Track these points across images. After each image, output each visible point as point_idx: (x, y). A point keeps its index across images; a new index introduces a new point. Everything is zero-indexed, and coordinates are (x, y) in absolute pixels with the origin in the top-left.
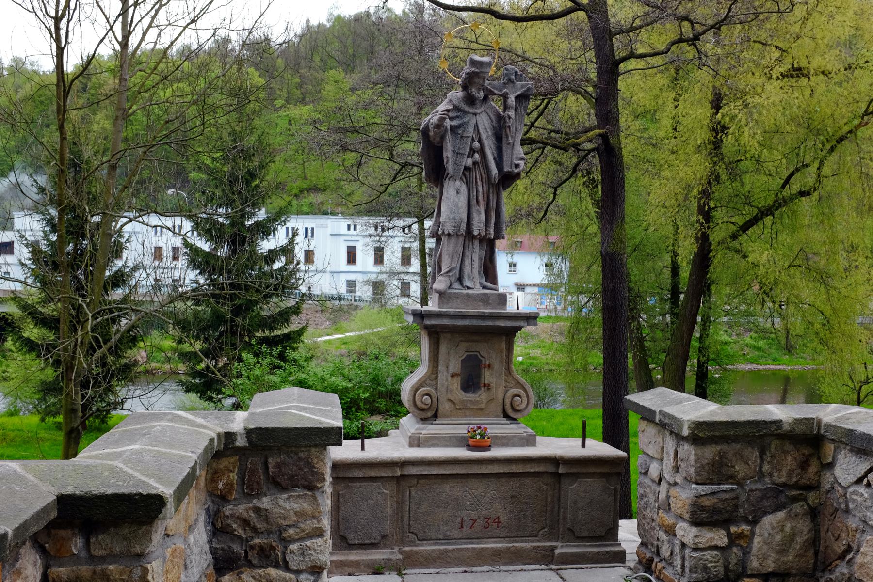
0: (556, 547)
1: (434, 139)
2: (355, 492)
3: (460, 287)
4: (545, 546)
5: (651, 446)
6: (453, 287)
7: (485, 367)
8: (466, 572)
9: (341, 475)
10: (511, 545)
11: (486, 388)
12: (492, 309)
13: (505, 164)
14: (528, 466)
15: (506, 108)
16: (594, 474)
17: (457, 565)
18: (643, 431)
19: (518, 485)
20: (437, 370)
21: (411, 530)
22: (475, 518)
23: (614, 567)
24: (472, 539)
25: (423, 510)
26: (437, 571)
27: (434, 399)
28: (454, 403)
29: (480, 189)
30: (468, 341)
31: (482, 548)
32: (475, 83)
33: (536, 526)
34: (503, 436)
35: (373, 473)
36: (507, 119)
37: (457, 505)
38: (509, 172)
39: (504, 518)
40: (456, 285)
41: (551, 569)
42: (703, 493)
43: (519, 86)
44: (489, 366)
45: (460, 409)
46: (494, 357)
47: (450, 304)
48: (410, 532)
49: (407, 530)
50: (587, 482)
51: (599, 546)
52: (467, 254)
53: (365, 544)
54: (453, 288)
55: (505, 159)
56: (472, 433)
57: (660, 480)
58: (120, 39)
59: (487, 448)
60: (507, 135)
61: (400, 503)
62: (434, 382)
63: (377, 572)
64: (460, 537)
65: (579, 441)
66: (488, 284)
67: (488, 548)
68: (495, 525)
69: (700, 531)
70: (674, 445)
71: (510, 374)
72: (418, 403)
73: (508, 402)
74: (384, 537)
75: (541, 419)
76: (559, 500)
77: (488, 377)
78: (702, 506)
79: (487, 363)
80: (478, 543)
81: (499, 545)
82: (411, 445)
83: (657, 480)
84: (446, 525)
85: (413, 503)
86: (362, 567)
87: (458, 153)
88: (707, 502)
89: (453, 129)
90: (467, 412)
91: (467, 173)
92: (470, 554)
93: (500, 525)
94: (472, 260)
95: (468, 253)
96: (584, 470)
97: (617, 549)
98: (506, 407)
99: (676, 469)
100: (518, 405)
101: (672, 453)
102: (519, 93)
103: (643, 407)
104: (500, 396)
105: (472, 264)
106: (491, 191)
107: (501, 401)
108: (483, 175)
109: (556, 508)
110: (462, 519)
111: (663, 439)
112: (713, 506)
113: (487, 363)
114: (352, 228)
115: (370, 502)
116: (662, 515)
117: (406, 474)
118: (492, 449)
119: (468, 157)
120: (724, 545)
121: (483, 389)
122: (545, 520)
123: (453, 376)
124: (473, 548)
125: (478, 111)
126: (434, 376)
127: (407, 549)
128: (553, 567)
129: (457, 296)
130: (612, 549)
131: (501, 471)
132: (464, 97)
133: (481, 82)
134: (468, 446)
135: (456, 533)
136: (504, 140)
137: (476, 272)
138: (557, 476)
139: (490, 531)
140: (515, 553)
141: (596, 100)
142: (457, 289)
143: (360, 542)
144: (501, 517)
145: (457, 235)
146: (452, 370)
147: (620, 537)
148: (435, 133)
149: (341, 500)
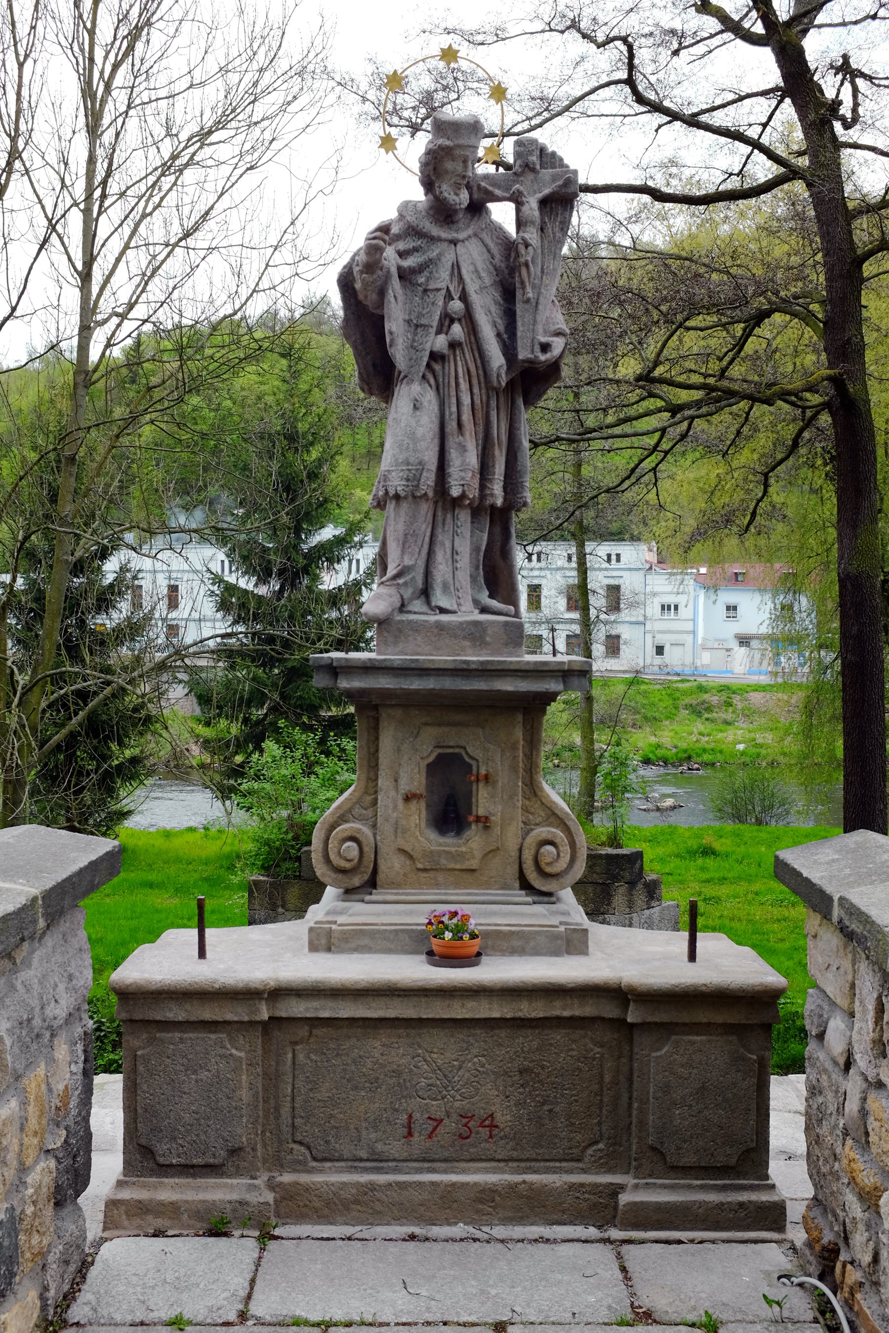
0: (622, 1187)
1: (366, 297)
3: (425, 609)
4: (597, 1185)
5: (830, 975)
6: (410, 608)
7: (478, 780)
8: (413, 1237)
9: (138, 1016)
10: (518, 1178)
11: (480, 825)
12: (491, 655)
13: (519, 343)
14: (558, 1003)
16: (709, 1024)
17: (398, 1220)
18: (815, 937)
19: (535, 1044)
21: (299, 1138)
22: (439, 1115)
23: (756, 1242)
24: (433, 1161)
26: (348, 1230)
27: (366, 849)
28: (411, 857)
29: (466, 400)
30: (439, 725)
31: (454, 1185)
32: (447, 172)
33: (579, 1137)
34: (512, 933)
35: (208, 1013)
36: (522, 249)
39: (503, 1118)
40: (418, 605)
41: (607, 1241)
43: (547, 178)
44: (487, 777)
45: (425, 870)
46: (498, 758)
47: (401, 645)
48: (295, 1142)
49: (289, 1136)
50: (693, 1043)
52: (440, 537)
53: (193, 1166)
54: (410, 612)
55: (519, 334)
56: (438, 926)
58: (80, 267)
59: (471, 960)
60: (522, 283)
63: (217, 1231)
66: (494, 604)
67: (467, 1184)
68: (484, 1132)
70: (876, 985)
71: (536, 795)
72: (332, 856)
73: (528, 856)
74: (234, 1152)
75: (758, 843)
76: (630, 1080)
79: (483, 771)
80: (445, 1172)
81: (492, 1178)
82: (314, 947)
83: (842, 1061)
84: (376, 1128)
86: (185, 1217)
87: (417, 326)
89: (404, 275)
90: (441, 878)
91: (437, 367)
92: (426, 1196)
93: (495, 1131)
94: (454, 552)
95: (444, 538)
96: (685, 1017)
97: (764, 1197)
98: (524, 866)
100: (549, 864)
101: (871, 1007)
103: (807, 880)
104: (512, 844)
105: (454, 561)
106: (493, 403)
107: (515, 854)
110: (410, 1117)
111: (853, 965)
113: (483, 771)
115: (204, 1075)
116: (852, 1155)
117: (284, 1014)
118: (484, 959)
119: (439, 332)
121: (473, 827)
122: (599, 1124)
123: (407, 799)
125: (461, 236)
126: (369, 798)
127: (287, 1178)
128: (615, 1234)
129: (417, 628)
131: (496, 1014)
132: (431, 208)
133: (460, 168)
134: (430, 953)
135: (395, 1148)
138: (620, 1024)
139: (473, 1145)
140: (528, 1198)
141: (825, 324)
142: (419, 613)
143: (182, 1161)
144: (498, 1116)
145: (414, 497)
146: (405, 785)
147: (771, 1171)
148: (366, 285)
149: (141, 1068)
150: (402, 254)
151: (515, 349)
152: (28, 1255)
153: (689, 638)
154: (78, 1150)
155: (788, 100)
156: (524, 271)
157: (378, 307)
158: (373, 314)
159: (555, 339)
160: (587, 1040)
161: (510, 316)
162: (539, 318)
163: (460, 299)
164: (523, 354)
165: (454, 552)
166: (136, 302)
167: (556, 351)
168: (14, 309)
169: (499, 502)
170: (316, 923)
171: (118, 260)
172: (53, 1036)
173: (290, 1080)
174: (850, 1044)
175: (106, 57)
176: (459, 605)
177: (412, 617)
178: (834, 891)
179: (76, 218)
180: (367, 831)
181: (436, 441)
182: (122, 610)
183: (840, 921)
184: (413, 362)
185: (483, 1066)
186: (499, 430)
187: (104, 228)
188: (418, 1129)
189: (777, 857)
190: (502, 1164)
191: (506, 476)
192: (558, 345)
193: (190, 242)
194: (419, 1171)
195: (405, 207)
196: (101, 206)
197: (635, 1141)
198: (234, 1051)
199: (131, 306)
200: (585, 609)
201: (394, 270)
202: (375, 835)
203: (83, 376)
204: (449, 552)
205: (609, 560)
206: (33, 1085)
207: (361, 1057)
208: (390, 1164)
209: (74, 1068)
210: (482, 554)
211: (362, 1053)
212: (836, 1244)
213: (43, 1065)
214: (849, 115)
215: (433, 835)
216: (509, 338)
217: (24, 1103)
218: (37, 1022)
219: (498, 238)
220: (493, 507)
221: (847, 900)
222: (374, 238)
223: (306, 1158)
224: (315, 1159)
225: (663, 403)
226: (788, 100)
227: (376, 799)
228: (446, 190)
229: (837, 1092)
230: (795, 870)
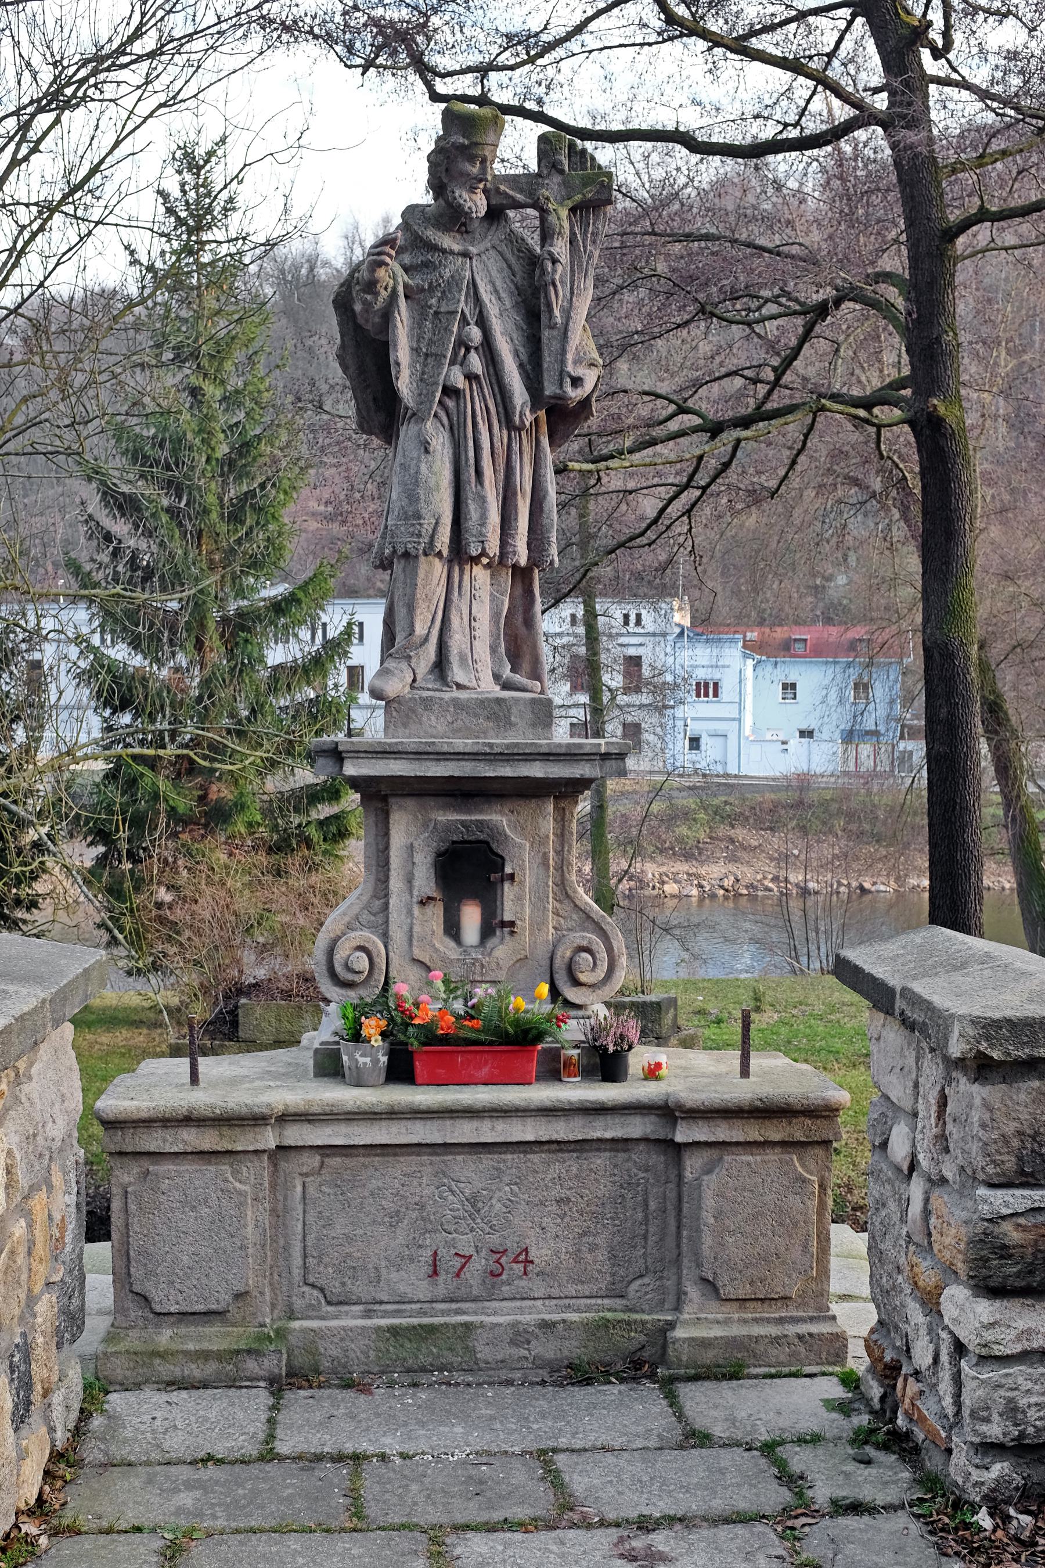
1: (367, 321)
15: (546, 235)
20: (387, 888)
21: (311, 1279)
27: (376, 960)
37: (423, 1219)
42: (1005, 1211)
48: (306, 1284)
55: (545, 366)
57: (912, 1168)
62: (380, 919)
65: (734, 1057)
72: (339, 968)
78: (1004, 1247)
83: (905, 1168)
88: (1011, 1234)
91: (450, 403)
93: (530, 1267)
94: (472, 618)
98: (556, 976)
99: (942, 1141)
107: (546, 963)
110: (436, 1253)
114: (633, 618)
119: (452, 363)
121: (498, 933)
126: (378, 904)
130: (815, 1328)
149: (132, 1207)
154: (73, 1291)
155: (860, 20)
157: (381, 332)
158: (374, 340)
159: (587, 371)
163: (477, 324)
169: (523, 561)
170: (322, 1044)
173: (301, 1217)
174: (914, 1145)
176: (478, 679)
178: (894, 981)
183: (902, 1013)
184: (424, 396)
188: (445, 1266)
189: (838, 956)
191: (531, 530)
195: (411, 212)
198: (237, 1185)
200: (595, 690)
204: (466, 618)
207: (379, 1189)
208: (414, 1306)
210: (503, 621)
211: (380, 1184)
212: (898, 1361)
214: (940, 43)
216: (533, 369)
217: (30, 1226)
219: (519, 251)
220: (515, 567)
221: (909, 990)
223: (320, 1303)
225: (700, 421)
226: (860, 20)
229: (900, 1199)
230: (856, 967)
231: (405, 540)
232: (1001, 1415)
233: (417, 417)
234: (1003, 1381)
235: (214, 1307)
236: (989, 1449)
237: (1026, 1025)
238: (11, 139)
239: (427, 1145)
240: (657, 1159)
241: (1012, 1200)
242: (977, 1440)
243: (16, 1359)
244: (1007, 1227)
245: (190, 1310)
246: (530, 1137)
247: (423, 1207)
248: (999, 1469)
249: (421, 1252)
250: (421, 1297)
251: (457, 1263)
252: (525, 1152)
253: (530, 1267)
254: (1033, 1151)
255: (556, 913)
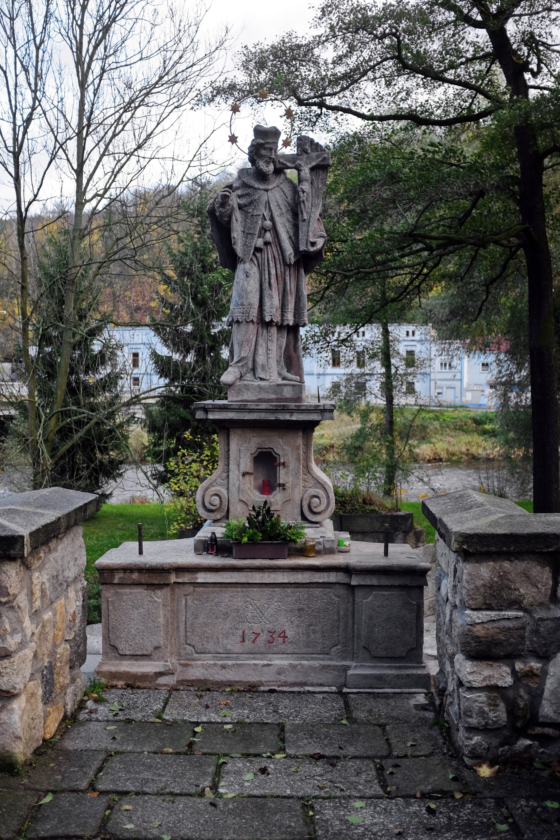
0: (348, 667)
2: (124, 599)
3: (253, 378)
4: (337, 666)
5: (443, 558)
11: (281, 488)
21: (189, 642)
25: (201, 620)
27: (223, 500)
29: (273, 272)
33: (328, 643)
37: (238, 616)
38: (305, 251)
40: (249, 376)
51: (400, 668)
58: (75, 167)
61: (175, 613)
64: (241, 651)
66: (289, 376)
68: (281, 640)
69: (476, 666)
72: (207, 504)
77: (283, 476)
80: (261, 659)
83: (445, 599)
85: (189, 612)
88: (479, 631)
89: (240, 207)
91: (258, 255)
93: (286, 640)
102: (314, 164)
105: (268, 354)
106: (287, 273)
108: (277, 256)
109: (350, 622)
110: (244, 632)
112: (492, 637)
119: (259, 237)
120: (506, 685)
121: (278, 489)
122: (338, 636)
123: (244, 475)
124: (255, 664)
125: (270, 187)
126: (225, 474)
130: (414, 672)
136: (300, 216)
137: (273, 363)
138: (351, 588)
139: (276, 646)
146: (243, 468)
149: (111, 607)
150: (239, 197)
151: (298, 245)
152: (58, 686)
153: (458, 384)
154: (80, 643)
156: (302, 205)
160: (332, 594)
161: (296, 227)
162: (310, 230)
163: (270, 220)
164: (302, 248)
165: (268, 349)
166: (109, 188)
167: (319, 246)
168: (36, 196)
171: (98, 163)
172: (68, 586)
173: (184, 614)
175: (89, 42)
177: (246, 382)
179: (72, 146)
180: (225, 492)
181: (258, 293)
182: (104, 371)
184: (245, 252)
185: (279, 607)
186: (291, 286)
187: (90, 143)
190: (290, 656)
192: (320, 243)
193: (141, 152)
194: (248, 659)
196: (87, 131)
197: (355, 644)
198: (156, 599)
199: (106, 190)
201: (236, 206)
202: (228, 493)
203: (78, 233)
205: (413, 333)
206: (59, 607)
208: (234, 655)
209: (78, 603)
210: (283, 350)
213: (63, 598)
214: (535, 70)
215: (257, 493)
216: (296, 239)
217: (55, 615)
218: (60, 577)
222: (225, 191)
224: (197, 653)
227: (228, 475)
228: (262, 165)
231: (237, 315)
232: (477, 714)
233: (243, 261)
234: (478, 699)
235: (145, 653)
236: (471, 729)
237: (485, 537)
238: (112, 125)
239: (240, 583)
240: (342, 591)
241: (481, 616)
242: (466, 725)
243: (45, 673)
244: (479, 627)
245: (134, 653)
246: (286, 581)
247: (238, 612)
248: (476, 739)
249: (237, 631)
250: (237, 651)
251: (253, 636)
252: (284, 588)
253: (286, 640)
254: (490, 594)
255: (304, 480)
